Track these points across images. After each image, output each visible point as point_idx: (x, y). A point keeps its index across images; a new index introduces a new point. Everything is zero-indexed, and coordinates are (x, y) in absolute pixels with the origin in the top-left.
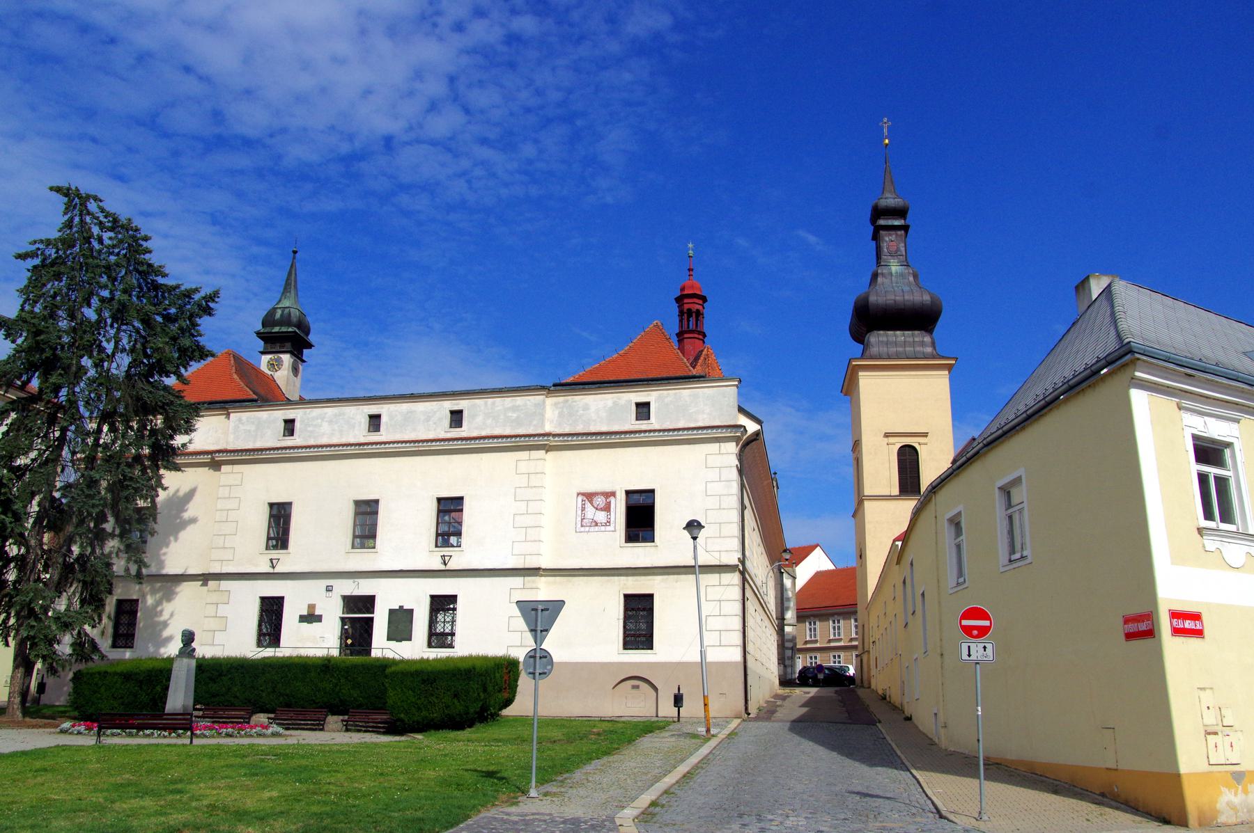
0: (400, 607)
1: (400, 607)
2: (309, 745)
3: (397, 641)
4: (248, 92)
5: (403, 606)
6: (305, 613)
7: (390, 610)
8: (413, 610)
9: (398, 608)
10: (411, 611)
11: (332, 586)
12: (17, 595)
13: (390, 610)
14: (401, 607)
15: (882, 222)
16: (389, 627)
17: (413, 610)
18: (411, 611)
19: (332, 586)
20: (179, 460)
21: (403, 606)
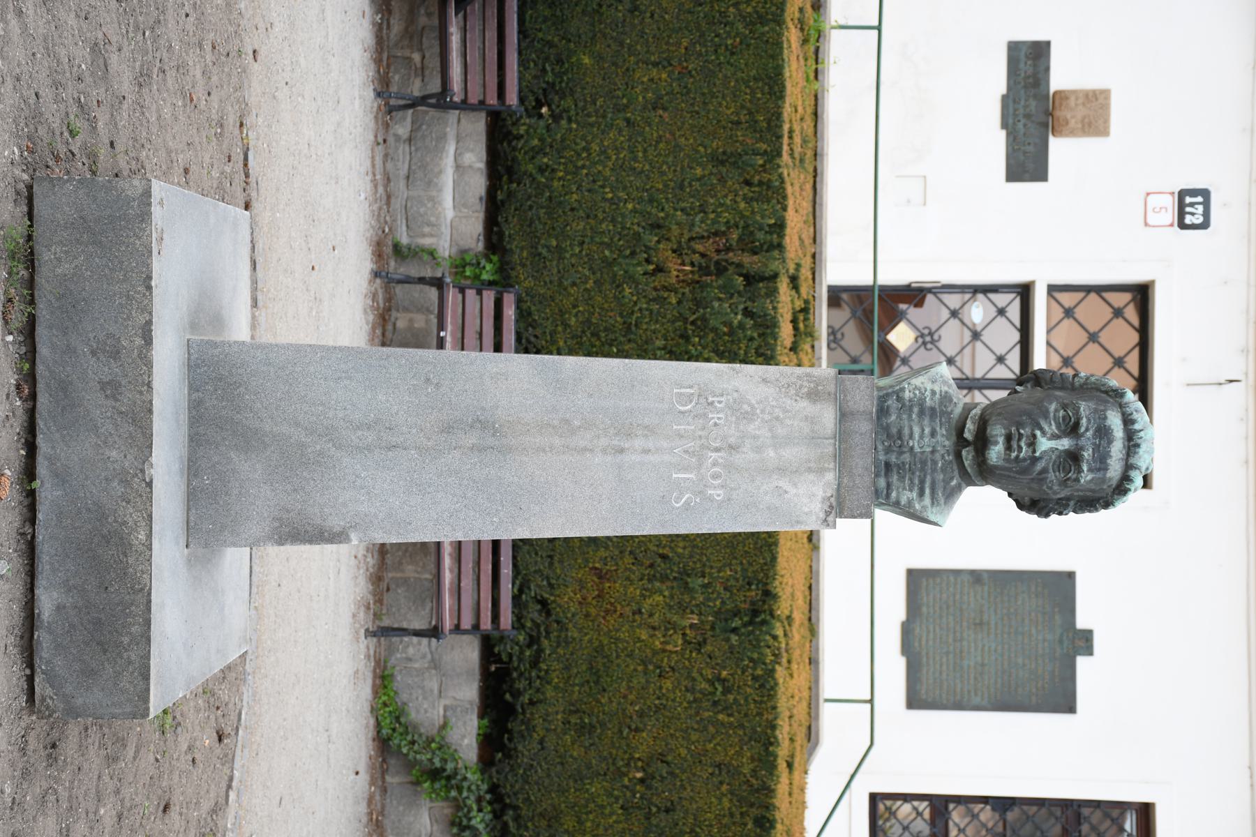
0: (1087, 636)
1: (1087, 636)
2: (783, 182)
3: (904, 625)
4: (356, 557)
5: (1089, 651)
6: (1061, 77)
7: (1069, 577)
8: (1071, 708)
9: (1082, 622)
10: (1063, 701)
11: (1205, 225)
12: (606, 558)
13: (1069, 577)
14: (1084, 642)
15: (448, 624)
16: (976, 576)
17: (1071, 708)
18: (1063, 701)
19: (1205, 225)
20: (1019, 290)
21: (1089, 651)
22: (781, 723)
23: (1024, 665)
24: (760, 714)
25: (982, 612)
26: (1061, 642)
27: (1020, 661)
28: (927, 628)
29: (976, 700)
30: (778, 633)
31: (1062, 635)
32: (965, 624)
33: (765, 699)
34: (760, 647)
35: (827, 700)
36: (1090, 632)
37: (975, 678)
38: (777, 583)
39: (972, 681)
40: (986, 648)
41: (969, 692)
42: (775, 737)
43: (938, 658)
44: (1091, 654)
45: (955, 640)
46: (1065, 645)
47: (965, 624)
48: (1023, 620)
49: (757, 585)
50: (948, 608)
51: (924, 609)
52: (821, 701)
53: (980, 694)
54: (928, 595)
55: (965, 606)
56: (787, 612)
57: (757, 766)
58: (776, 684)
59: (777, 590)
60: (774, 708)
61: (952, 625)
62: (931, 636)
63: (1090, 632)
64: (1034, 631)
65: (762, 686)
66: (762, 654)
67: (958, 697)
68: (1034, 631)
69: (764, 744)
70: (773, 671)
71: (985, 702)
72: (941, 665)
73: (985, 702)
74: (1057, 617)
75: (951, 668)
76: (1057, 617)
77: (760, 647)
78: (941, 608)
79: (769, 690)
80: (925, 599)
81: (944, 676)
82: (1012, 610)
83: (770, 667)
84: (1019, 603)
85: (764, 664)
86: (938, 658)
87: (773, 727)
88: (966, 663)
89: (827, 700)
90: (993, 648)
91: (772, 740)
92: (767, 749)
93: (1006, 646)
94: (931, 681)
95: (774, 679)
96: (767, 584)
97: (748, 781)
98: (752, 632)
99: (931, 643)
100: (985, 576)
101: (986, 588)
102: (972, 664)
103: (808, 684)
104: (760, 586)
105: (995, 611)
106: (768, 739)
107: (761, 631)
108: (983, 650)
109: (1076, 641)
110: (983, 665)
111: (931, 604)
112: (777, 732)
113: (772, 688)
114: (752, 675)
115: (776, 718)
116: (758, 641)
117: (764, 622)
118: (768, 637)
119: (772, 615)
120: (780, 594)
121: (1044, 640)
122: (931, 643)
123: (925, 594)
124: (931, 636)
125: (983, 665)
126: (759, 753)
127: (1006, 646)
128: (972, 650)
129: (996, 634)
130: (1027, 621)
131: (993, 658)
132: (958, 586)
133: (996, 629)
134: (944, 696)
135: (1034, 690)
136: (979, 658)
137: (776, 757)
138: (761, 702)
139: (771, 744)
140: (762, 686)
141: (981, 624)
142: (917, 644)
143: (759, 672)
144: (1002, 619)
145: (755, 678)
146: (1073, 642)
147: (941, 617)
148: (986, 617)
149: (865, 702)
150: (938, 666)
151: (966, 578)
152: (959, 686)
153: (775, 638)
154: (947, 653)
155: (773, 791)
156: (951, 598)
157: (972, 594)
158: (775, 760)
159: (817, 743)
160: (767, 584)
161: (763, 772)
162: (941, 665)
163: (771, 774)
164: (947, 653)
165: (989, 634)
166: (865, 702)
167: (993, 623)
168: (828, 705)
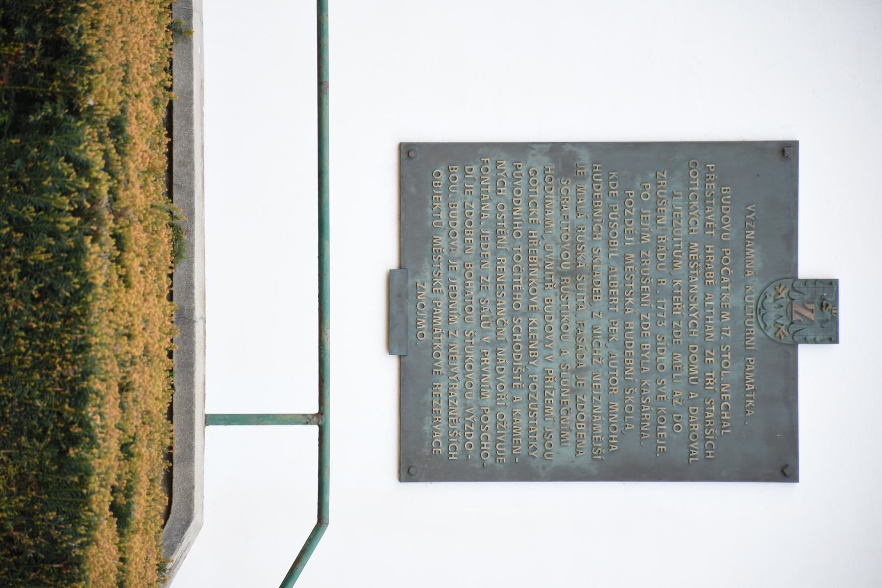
22: (98, 386)
23: (674, 369)
24: (40, 365)
25: (576, 244)
26: (760, 310)
27: (665, 359)
28: (448, 284)
29: (564, 455)
30: (90, 155)
31: (763, 294)
32: (537, 273)
33: (58, 324)
34: (42, 191)
35: (212, 420)
36: (832, 285)
37: (561, 403)
38: (84, 21)
39: (553, 410)
40: (587, 331)
41: (546, 434)
42: (84, 424)
43: (473, 356)
44: (833, 339)
45: (513, 314)
46: (772, 316)
47: (537, 273)
48: (673, 260)
49: (29, 26)
50: (497, 235)
51: (442, 241)
52: (199, 421)
53: (571, 437)
54: (450, 207)
55: (537, 232)
56: (112, 107)
57: (34, 501)
58: (88, 286)
59: (85, 39)
60: (82, 348)
61: (506, 276)
62: (458, 301)
63: (832, 285)
64: (698, 288)
65: (49, 291)
66: (46, 209)
67: (521, 449)
68: (698, 288)
69: (55, 442)
70: (79, 251)
71: (584, 460)
72: (481, 375)
73: (584, 460)
74: (753, 252)
75: (504, 378)
76: (753, 252)
77: (42, 191)
78: (480, 237)
79: (65, 302)
80: (443, 215)
81: (489, 400)
82: (647, 238)
83: (70, 243)
84: (665, 219)
85: (55, 234)
86: (473, 356)
87: (80, 397)
88: (539, 366)
89: (212, 420)
90: (603, 328)
91: (76, 430)
92: (63, 453)
93: (633, 324)
94: (458, 412)
95: (80, 272)
96: (56, 23)
97: (10, 539)
98: (21, 151)
99: (457, 321)
100: (585, 157)
101: (587, 186)
102: (554, 367)
103: (166, 343)
104: (38, 28)
105: (608, 243)
106: (66, 430)
107: (44, 147)
108: (577, 335)
109: (797, 308)
110: (578, 370)
111: (458, 229)
112: (90, 410)
113: (76, 297)
114: (23, 263)
115: (85, 375)
116: (37, 174)
117: (50, 126)
118: (61, 165)
119: (74, 111)
120: (92, 52)
121: (722, 309)
122: (457, 321)
123: (442, 205)
124: (458, 301)
125: (578, 370)
126: (41, 467)
127: (633, 324)
128: (555, 333)
129: (610, 295)
130: (681, 264)
131: (603, 353)
132: (522, 183)
133: (610, 286)
134: (488, 446)
135: (698, 427)
136: (570, 354)
137: (85, 473)
138: (47, 332)
139: (74, 441)
140: (49, 291)
141: (574, 273)
142: (424, 325)
143: (40, 256)
144: (625, 259)
145: (29, 272)
146: (790, 313)
147: (481, 258)
148: (585, 258)
149: (306, 419)
150: (473, 376)
151: (539, 163)
152: (523, 421)
153: (83, 168)
154: (496, 344)
155: (78, 562)
156: (506, 213)
157: (554, 203)
158: (83, 483)
159: (187, 521)
160: (56, 23)
161: (52, 515)
162: (481, 375)
163: (74, 519)
164: (496, 344)
165: (592, 295)
166: (306, 419)
167: (602, 269)
168: (210, 429)
